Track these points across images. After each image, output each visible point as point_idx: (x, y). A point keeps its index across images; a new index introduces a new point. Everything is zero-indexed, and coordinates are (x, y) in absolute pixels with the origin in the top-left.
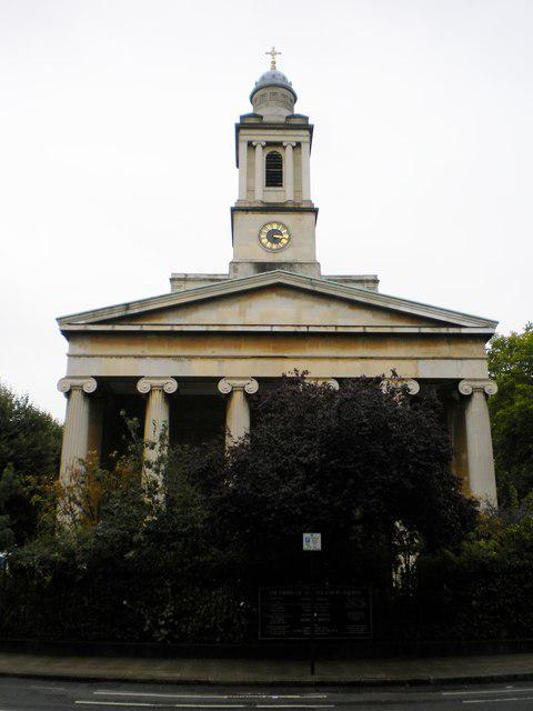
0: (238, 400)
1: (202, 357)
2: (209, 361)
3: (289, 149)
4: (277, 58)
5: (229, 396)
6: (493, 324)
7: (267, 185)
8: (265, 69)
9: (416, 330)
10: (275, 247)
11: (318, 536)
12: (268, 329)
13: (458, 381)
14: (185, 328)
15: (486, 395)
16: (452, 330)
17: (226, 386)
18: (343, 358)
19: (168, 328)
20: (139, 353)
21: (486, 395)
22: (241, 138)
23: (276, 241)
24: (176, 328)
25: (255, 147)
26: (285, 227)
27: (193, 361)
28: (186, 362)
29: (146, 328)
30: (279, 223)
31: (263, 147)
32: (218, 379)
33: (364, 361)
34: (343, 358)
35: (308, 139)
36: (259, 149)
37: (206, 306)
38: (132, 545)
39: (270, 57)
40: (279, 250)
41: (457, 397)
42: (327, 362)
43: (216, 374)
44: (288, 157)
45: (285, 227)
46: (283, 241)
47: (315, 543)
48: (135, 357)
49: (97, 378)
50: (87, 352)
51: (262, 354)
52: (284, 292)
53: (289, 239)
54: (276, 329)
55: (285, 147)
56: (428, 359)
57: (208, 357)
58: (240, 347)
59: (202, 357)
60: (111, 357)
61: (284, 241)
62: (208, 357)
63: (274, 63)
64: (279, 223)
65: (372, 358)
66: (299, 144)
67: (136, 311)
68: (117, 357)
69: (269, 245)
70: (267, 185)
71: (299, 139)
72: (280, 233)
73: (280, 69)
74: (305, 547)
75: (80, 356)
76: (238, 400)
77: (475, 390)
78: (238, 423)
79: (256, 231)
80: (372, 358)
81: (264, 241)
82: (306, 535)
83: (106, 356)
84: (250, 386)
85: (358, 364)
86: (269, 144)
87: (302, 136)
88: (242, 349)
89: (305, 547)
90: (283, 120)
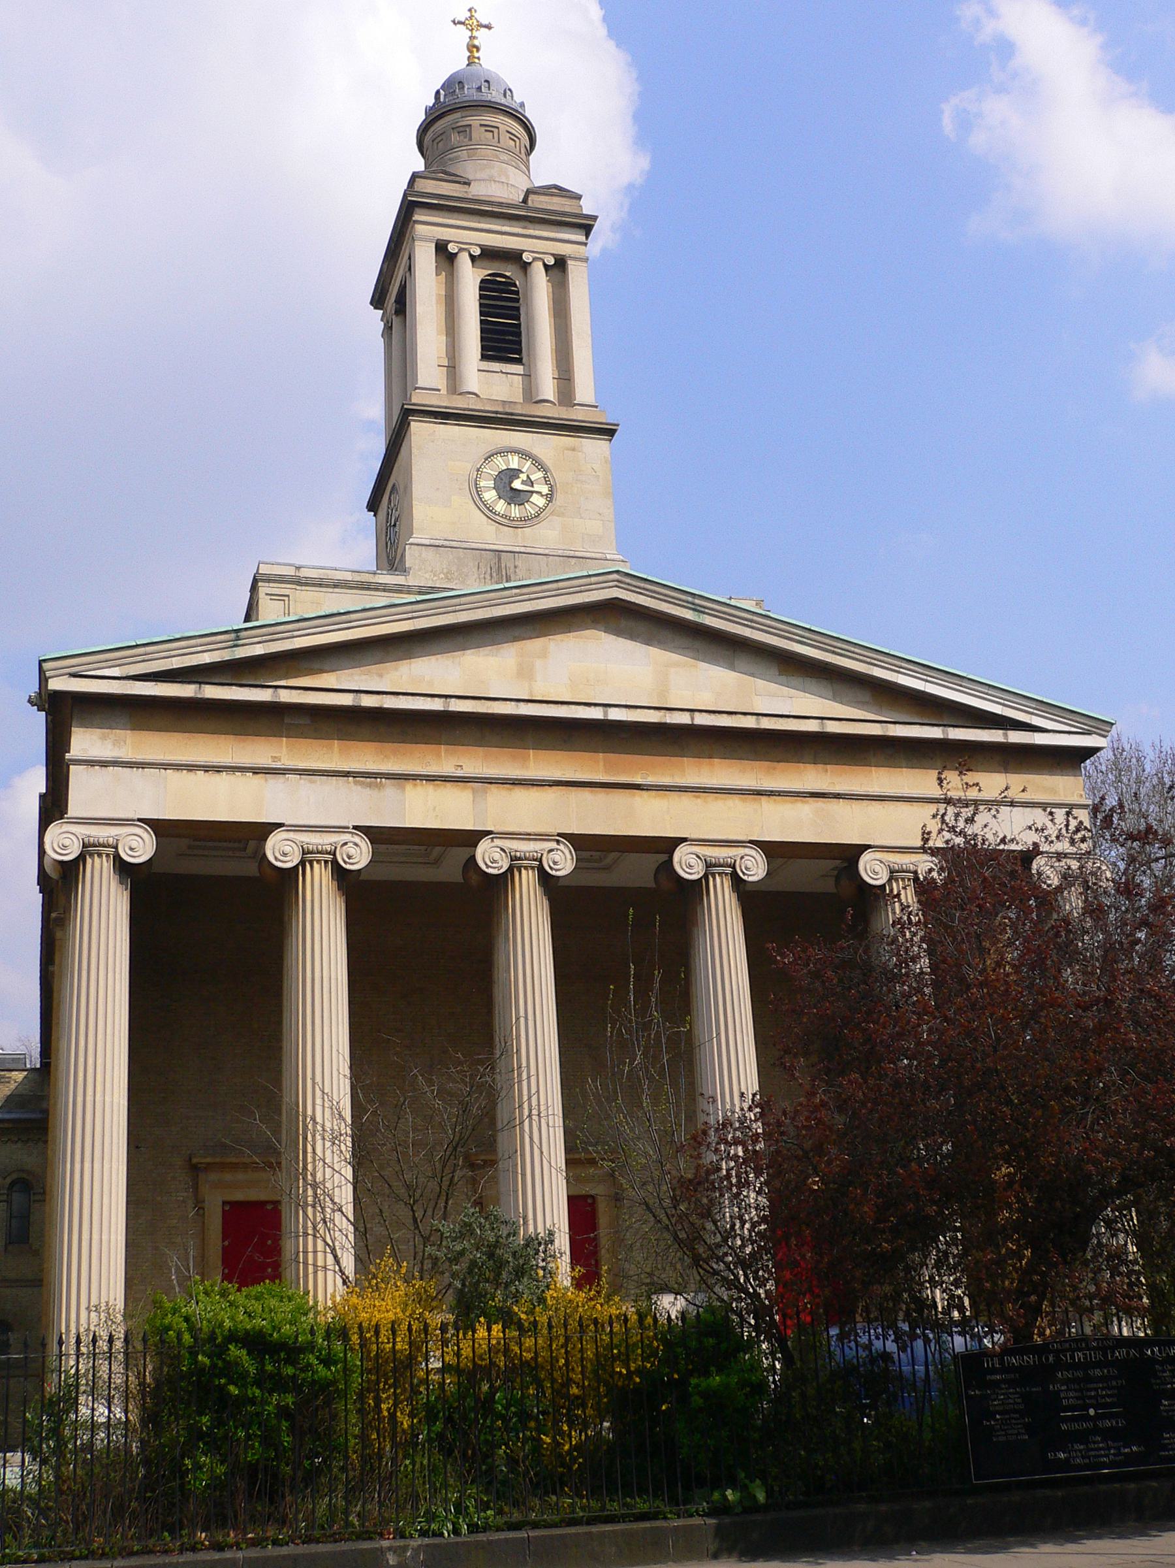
0: (527, 883)
1: (431, 779)
4: (482, 35)
6: (1101, 726)
7: (481, 360)
8: (457, 62)
9: (935, 733)
10: (515, 511)
12: (596, 714)
14: (390, 703)
16: (1016, 737)
17: (693, 860)
18: (771, 793)
19: (346, 700)
20: (264, 761)
23: (516, 497)
24: (368, 701)
26: (539, 465)
27: (409, 786)
28: (390, 789)
29: (286, 697)
30: (525, 455)
32: (473, 838)
33: (820, 803)
34: (771, 793)
36: (464, 261)
39: (463, 34)
40: (527, 520)
42: (734, 802)
43: (467, 823)
45: (539, 465)
46: (535, 498)
48: (256, 771)
50: (126, 753)
54: (615, 715)
56: (242, 769)
57: (446, 779)
58: (526, 759)
59: (431, 779)
60: (191, 768)
61: (538, 500)
62: (446, 779)
63: (473, 48)
64: (525, 455)
65: (837, 796)
67: (259, 650)
68: (207, 769)
69: (501, 506)
70: (481, 360)
72: (514, 473)
73: (489, 61)
75: (104, 764)
76: (527, 883)
79: (465, 467)
80: (837, 796)
81: (490, 495)
83: (178, 767)
84: (556, 856)
85: (807, 809)
86: (489, 254)
87: (564, 243)
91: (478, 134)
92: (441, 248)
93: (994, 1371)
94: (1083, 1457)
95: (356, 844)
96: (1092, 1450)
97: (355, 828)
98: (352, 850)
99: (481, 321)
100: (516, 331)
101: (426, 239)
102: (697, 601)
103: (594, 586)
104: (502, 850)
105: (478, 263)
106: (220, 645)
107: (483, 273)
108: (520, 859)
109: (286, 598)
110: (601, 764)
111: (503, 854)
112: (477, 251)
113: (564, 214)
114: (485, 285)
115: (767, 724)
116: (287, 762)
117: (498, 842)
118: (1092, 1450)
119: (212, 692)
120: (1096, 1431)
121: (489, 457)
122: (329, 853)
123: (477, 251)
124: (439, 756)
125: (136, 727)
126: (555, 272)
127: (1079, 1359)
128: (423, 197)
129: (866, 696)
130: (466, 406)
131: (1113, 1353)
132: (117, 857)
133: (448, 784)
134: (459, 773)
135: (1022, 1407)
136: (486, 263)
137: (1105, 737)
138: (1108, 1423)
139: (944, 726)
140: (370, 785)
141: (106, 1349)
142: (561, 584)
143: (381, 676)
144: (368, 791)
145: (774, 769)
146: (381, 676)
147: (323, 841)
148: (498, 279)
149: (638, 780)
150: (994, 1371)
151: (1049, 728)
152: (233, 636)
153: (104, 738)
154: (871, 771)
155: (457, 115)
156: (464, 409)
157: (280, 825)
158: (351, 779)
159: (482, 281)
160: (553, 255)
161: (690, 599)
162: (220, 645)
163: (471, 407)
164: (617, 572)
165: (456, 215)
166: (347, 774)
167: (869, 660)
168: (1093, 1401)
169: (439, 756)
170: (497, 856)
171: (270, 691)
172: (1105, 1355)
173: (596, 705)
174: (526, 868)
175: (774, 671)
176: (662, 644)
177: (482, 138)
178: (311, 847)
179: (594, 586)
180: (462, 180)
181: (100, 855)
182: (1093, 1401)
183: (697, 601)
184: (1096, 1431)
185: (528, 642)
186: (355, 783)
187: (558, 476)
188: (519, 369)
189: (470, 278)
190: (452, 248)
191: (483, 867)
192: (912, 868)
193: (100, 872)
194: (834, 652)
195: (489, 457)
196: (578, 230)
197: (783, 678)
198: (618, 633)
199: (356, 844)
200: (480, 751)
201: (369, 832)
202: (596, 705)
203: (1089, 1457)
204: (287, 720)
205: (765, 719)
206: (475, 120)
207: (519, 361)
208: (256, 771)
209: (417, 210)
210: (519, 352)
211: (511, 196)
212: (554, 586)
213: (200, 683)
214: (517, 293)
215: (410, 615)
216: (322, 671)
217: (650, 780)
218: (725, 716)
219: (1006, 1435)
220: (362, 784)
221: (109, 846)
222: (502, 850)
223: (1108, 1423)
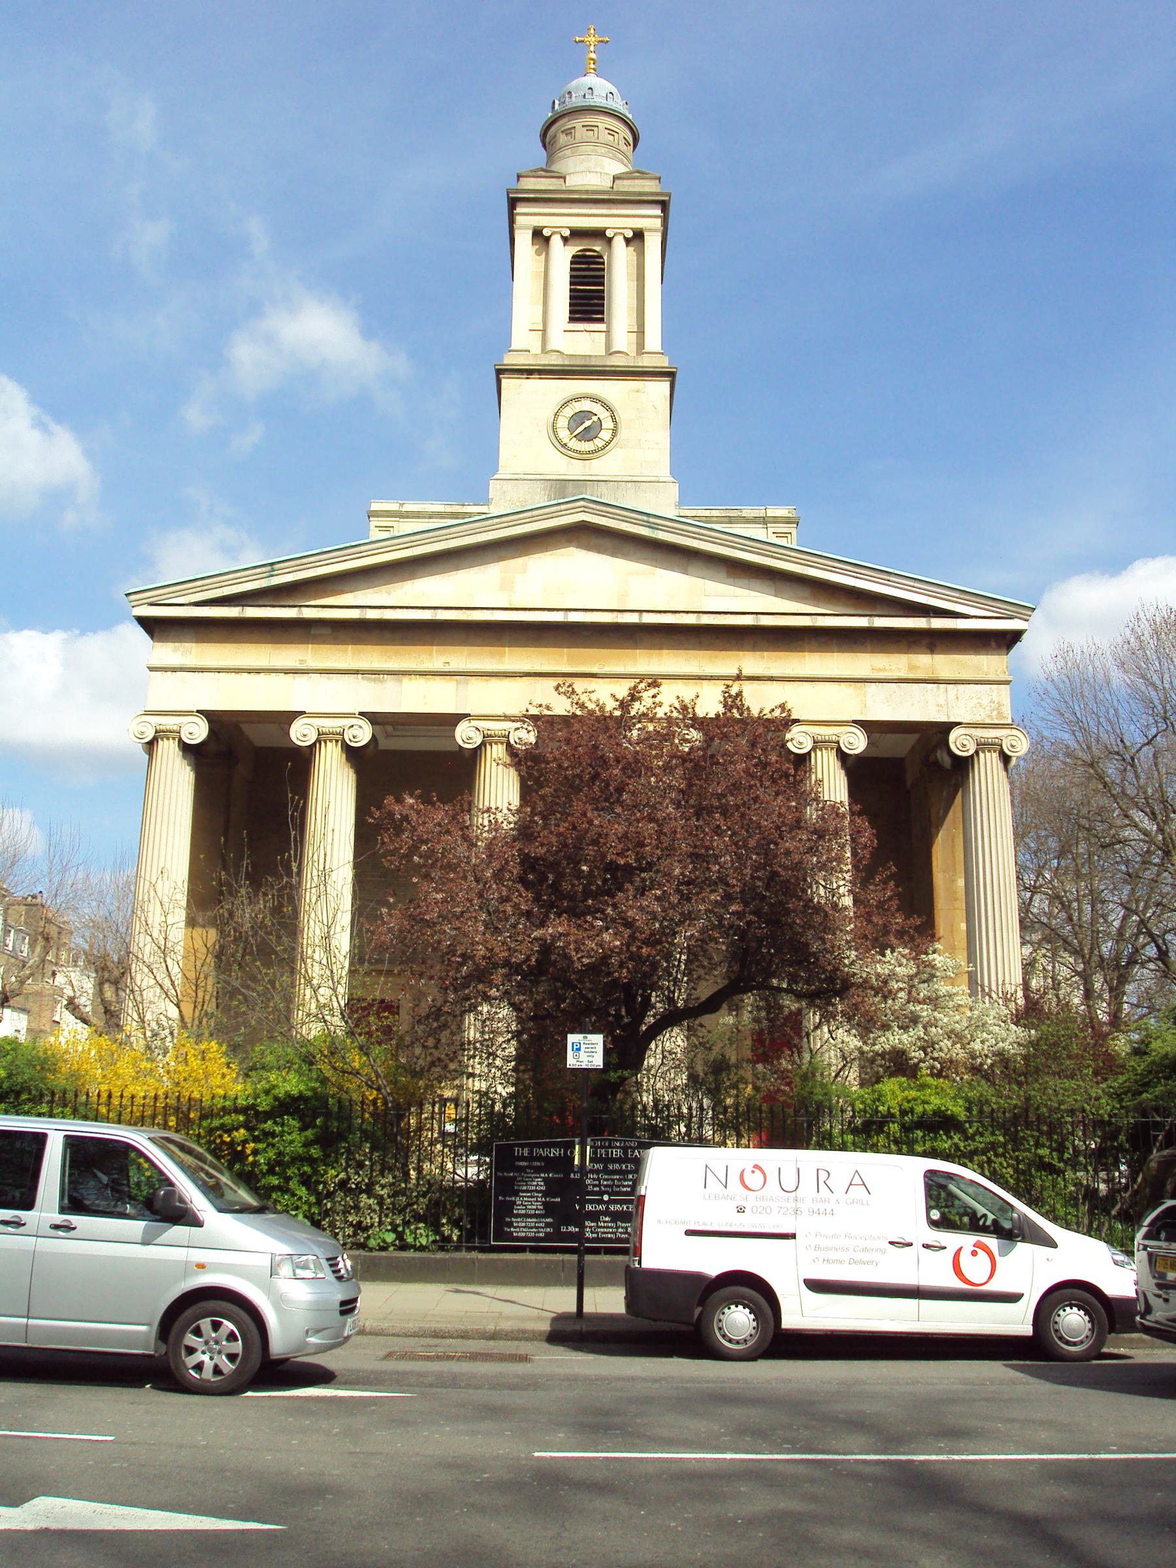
2: (438, 680)
3: (619, 243)
5: (476, 754)
7: (572, 320)
11: (598, 1039)
13: (948, 727)
15: (1005, 759)
16: (938, 623)
17: (473, 733)
21: (1005, 759)
22: (520, 220)
23: (588, 435)
25: (547, 240)
26: (608, 408)
27: (406, 680)
28: (390, 681)
29: (308, 613)
30: (595, 399)
31: (565, 240)
32: (454, 719)
35: (658, 223)
36: (556, 241)
37: (546, 549)
38: (462, 1511)
41: (947, 761)
44: (620, 259)
47: (591, 1053)
48: (287, 672)
49: (209, 715)
51: (538, 668)
52: (594, 541)
53: (615, 432)
55: (609, 241)
58: (502, 655)
65: (771, 679)
66: (638, 236)
70: (572, 320)
71: (639, 223)
72: (588, 414)
74: (571, 1062)
75: (174, 670)
77: (983, 746)
78: (418, 792)
80: (771, 679)
82: (572, 1038)
84: (355, 731)
86: (577, 234)
88: (506, 659)
89: (571, 1062)
90: (606, 183)
91: (581, 133)
92: (537, 234)
93: (523, 1158)
94: (592, 1232)
95: (360, 727)
96: (601, 1227)
97: (361, 714)
98: (355, 731)
99: (571, 290)
100: (600, 295)
101: (525, 228)
102: (651, 520)
103: (564, 513)
104: (477, 729)
105: (570, 242)
106: (259, 576)
107: (573, 249)
108: (491, 736)
109: (789, 535)
110: (565, 658)
111: (477, 732)
112: (567, 233)
113: (640, 194)
114: (576, 260)
115: (706, 620)
116: (312, 664)
117: (474, 723)
118: (601, 1227)
119: (252, 612)
120: (606, 1213)
121: (565, 404)
122: (339, 734)
123: (567, 233)
124: (431, 655)
125: (199, 640)
126: (637, 243)
127: (601, 1155)
128: (516, 193)
129: (806, 592)
130: (547, 363)
131: (633, 1152)
132: (180, 740)
133: (437, 677)
134: (447, 668)
135: (543, 1188)
136: (577, 241)
137: (1027, 620)
138: (618, 1207)
139: (871, 616)
140: (374, 680)
141: (152, 1103)
142: (535, 513)
143: (389, 593)
144: (373, 684)
145: (716, 657)
146: (389, 593)
147: (169, 722)
148: (588, 253)
149: (594, 669)
150: (523, 1158)
151: (972, 614)
152: (269, 568)
153: (175, 650)
154: (347, 650)
155: (565, 120)
156: (544, 365)
157: (959, 724)
158: (360, 676)
159: (574, 257)
160: (631, 229)
161: (645, 518)
162: (259, 576)
163: (553, 363)
164: (583, 499)
165: (551, 205)
166: (356, 672)
167: (803, 562)
168: (609, 1189)
169: (431, 655)
170: (471, 734)
171: (296, 609)
172: (625, 1153)
173: (558, 610)
174: (496, 743)
175: (723, 574)
176: (625, 556)
177: (584, 136)
178: (324, 730)
179: (564, 513)
180: (557, 175)
181: (826, 749)
182: (609, 1189)
183: (651, 520)
184: (606, 1213)
185: (512, 561)
186: (363, 679)
187: (622, 415)
188: (601, 327)
189: (562, 256)
190: (546, 232)
191: (461, 743)
192: (834, 738)
193: (168, 750)
194: (772, 557)
195: (565, 404)
196: (654, 206)
197: (731, 580)
198: (589, 548)
199: (360, 727)
200: (466, 649)
201: (865, 725)
202: (558, 610)
203: (597, 1233)
204: (313, 631)
205: (706, 616)
206: (578, 123)
207: (601, 320)
208: (287, 672)
209: (519, 204)
210: (602, 313)
211: (603, 184)
212: (529, 514)
213: (243, 606)
214: (603, 263)
215: (409, 545)
216: (342, 592)
217: (607, 669)
218: (670, 614)
219: (526, 1209)
220: (369, 679)
221: (174, 732)
222: (477, 729)
223: (618, 1207)
